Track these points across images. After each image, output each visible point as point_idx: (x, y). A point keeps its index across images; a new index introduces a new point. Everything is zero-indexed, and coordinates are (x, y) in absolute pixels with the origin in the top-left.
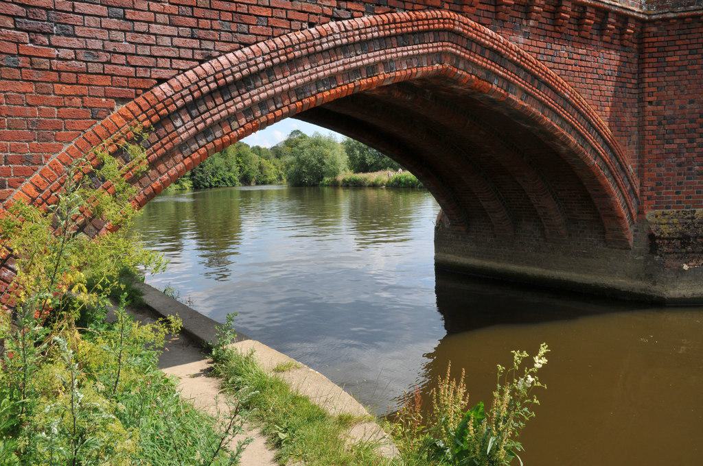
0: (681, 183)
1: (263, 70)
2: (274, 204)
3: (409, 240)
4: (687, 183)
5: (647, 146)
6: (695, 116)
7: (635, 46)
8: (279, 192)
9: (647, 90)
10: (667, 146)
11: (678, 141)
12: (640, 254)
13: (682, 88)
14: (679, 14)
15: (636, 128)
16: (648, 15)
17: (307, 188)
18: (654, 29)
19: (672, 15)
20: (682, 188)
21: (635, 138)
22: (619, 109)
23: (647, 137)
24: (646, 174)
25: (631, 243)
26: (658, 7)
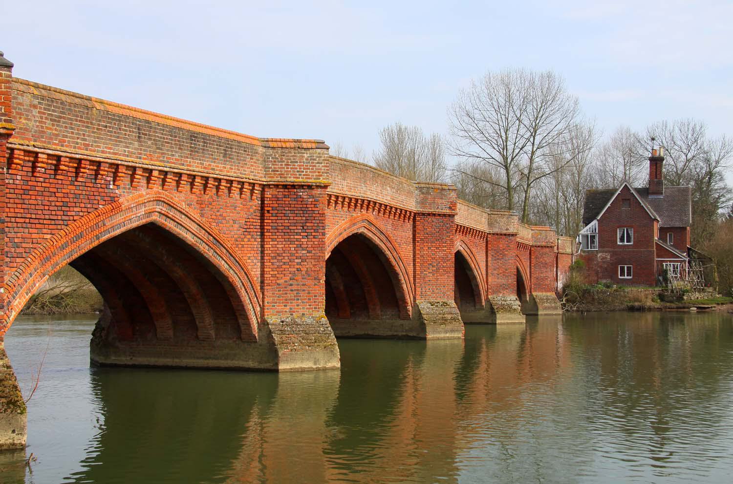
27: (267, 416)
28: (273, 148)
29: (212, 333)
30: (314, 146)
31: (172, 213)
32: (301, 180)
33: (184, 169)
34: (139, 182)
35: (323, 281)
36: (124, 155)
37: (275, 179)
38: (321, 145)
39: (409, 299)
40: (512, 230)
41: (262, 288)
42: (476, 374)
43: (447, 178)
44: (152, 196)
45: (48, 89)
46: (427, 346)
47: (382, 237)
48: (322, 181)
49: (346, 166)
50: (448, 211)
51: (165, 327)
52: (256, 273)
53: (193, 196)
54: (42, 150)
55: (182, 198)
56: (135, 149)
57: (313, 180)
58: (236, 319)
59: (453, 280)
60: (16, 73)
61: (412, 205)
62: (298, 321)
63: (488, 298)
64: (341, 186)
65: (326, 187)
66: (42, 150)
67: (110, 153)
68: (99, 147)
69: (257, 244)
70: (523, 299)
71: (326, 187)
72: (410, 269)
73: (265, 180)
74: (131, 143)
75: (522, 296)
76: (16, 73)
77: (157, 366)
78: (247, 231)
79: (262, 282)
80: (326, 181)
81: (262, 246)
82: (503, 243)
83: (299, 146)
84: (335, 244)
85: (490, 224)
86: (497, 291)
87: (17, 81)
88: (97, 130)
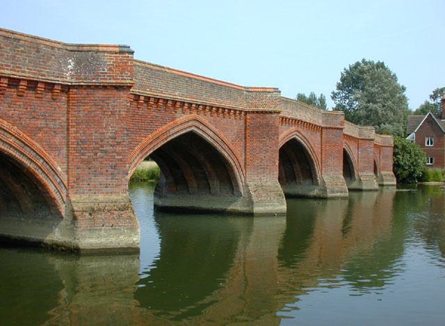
21: (64, 151)
28: (251, 92)
29: (218, 190)
30: (273, 90)
32: (266, 109)
33: (208, 103)
34: (57, 96)
35: (277, 164)
38: (277, 91)
39: (319, 175)
40: (371, 138)
41: (245, 167)
42: (349, 228)
43: (405, 177)
45: (289, 105)
46: (316, 232)
47: (305, 140)
48: (277, 109)
49: (287, 101)
50: (339, 126)
51: (215, 184)
52: (242, 159)
53: (212, 118)
55: (205, 118)
58: (231, 183)
59: (342, 164)
60: (135, 57)
62: (264, 184)
64: (286, 112)
65: (279, 112)
69: (242, 144)
71: (279, 112)
72: (319, 157)
73: (247, 109)
76: (135, 57)
78: (238, 136)
79: (245, 164)
81: (245, 144)
82: (367, 144)
83: (265, 91)
85: (360, 134)
86: (362, 171)
87: (136, 61)
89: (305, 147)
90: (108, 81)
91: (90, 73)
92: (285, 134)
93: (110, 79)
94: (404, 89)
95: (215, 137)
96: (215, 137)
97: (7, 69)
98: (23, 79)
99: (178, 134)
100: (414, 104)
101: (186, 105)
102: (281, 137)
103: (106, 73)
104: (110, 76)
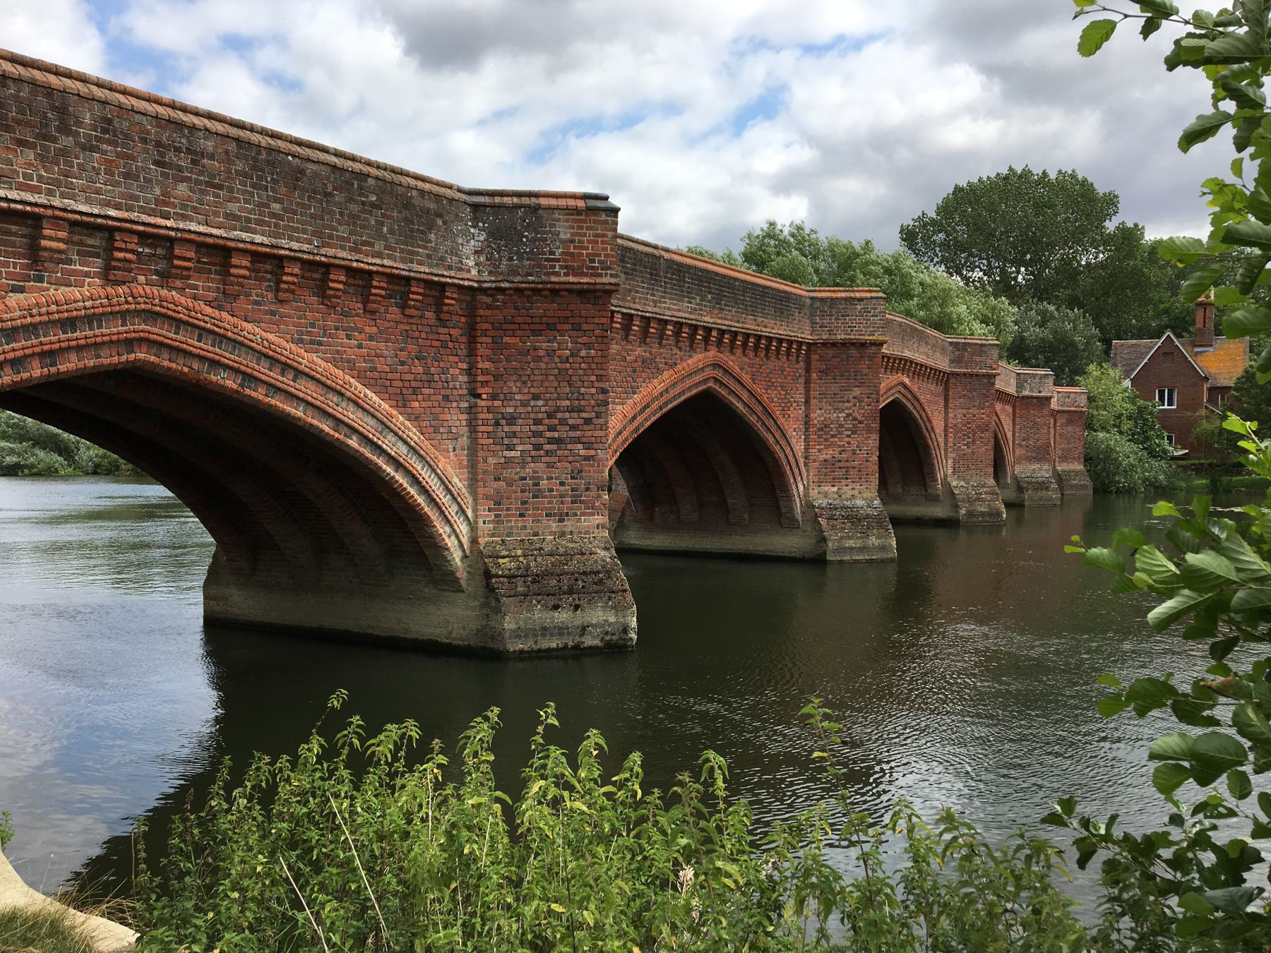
0: (525, 502)
1: (73, 347)
2: (158, 581)
3: (100, 497)
4: (534, 503)
5: (481, 453)
6: (540, 416)
7: (463, 319)
8: (625, 630)
9: (480, 378)
10: (507, 454)
11: (520, 448)
12: (475, 598)
13: (524, 378)
14: (514, 285)
15: (466, 428)
16: (477, 282)
17: (1196, 495)
18: (488, 300)
19: (506, 285)
20: (527, 509)
21: (464, 441)
22: (436, 404)
23: (481, 441)
24: (481, 490)
25: (463, 583)
26: (490, 273)
27: (182, 782)
31: (726, 380)
36: (687, 312)
37: (824, 337)
44: (710, 360)
53: (746, 359)
54: (618, 309)
56: (697, 304)
57: (867, 338)
58: (776, 499)
61: (943, 364)
63: (1013, 474)
66: (618, 309)
67: (675, 310)
68: (665, 303)
70: (1001, 480)
74: (693, 298)
75: (1000, 475)
77: (767, 556)
80: (881, 338)
84: (628, 436)
87: (622, 237)
88: (29, 276)
89: (910, 413)
90: (563, 279)
91: (521, 258)
92: (889, 385)
93: (566, 275)
94: (1011, 169)
95: (753, 403)
96: (753, 403)
97: (343, 248)
98: (378, 273)
99: (682, 398)
100: (1139, 841)
101: (670, 327)
102: (615, 423)
103: (558, 260)
104: (566, 267)
